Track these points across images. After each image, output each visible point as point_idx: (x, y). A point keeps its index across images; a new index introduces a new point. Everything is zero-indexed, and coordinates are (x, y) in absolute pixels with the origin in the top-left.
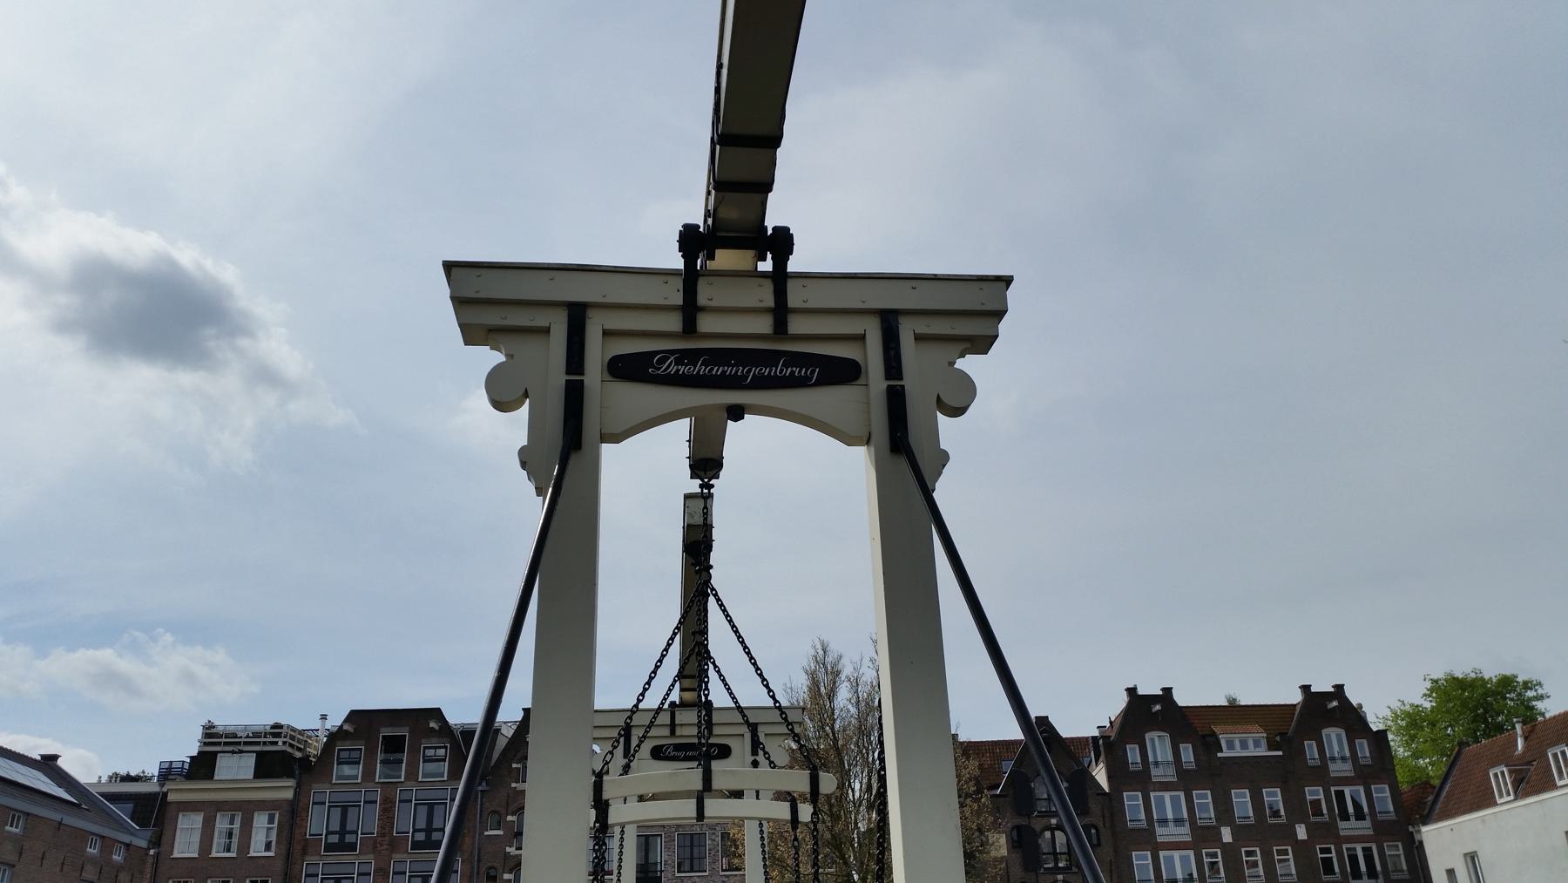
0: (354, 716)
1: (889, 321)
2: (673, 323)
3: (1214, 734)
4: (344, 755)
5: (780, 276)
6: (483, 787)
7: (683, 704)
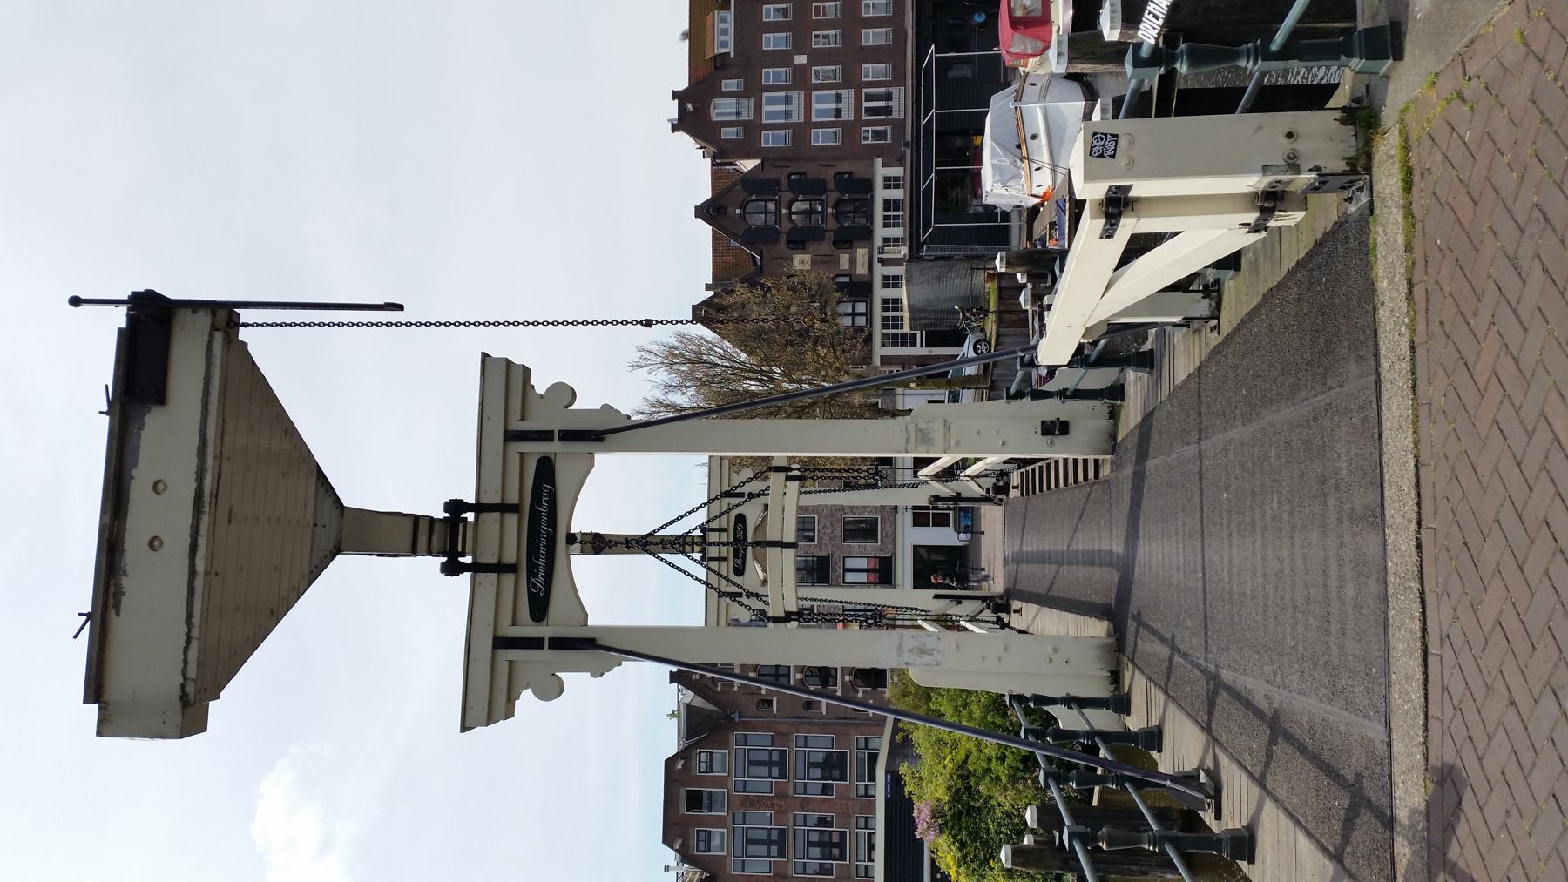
0: (668, 840)
1: (511, 436)
2: (508, 579)
3: (715, 57)
4: (702, 846)
5: (478, 508)
6: (735, 716)
7: (703, 551)
